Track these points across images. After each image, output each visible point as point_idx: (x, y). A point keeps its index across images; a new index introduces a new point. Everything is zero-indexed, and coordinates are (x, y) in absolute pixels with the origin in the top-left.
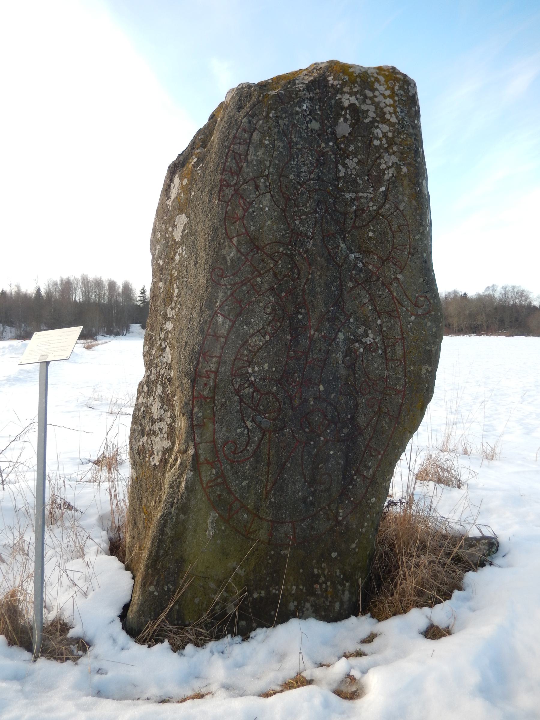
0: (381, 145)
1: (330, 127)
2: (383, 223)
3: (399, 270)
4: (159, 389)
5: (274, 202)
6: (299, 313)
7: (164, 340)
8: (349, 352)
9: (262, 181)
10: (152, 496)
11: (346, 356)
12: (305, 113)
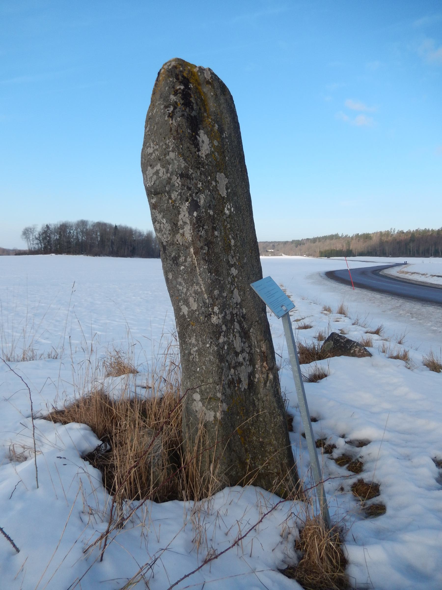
7: (232, 283)
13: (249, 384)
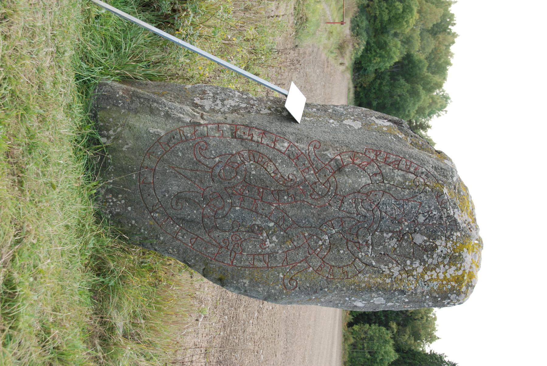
0: (406, 265)
1: (420, 230)
2: (349, 261)
3: (315, 269)
4: (243, 105)
5: (365, 186)
6: (289, 197)
8: (261, 229)
9: (380, 179)
10: (174, 98)
11: (258, 226)
12: (430, 213)
13: (197, 104)
